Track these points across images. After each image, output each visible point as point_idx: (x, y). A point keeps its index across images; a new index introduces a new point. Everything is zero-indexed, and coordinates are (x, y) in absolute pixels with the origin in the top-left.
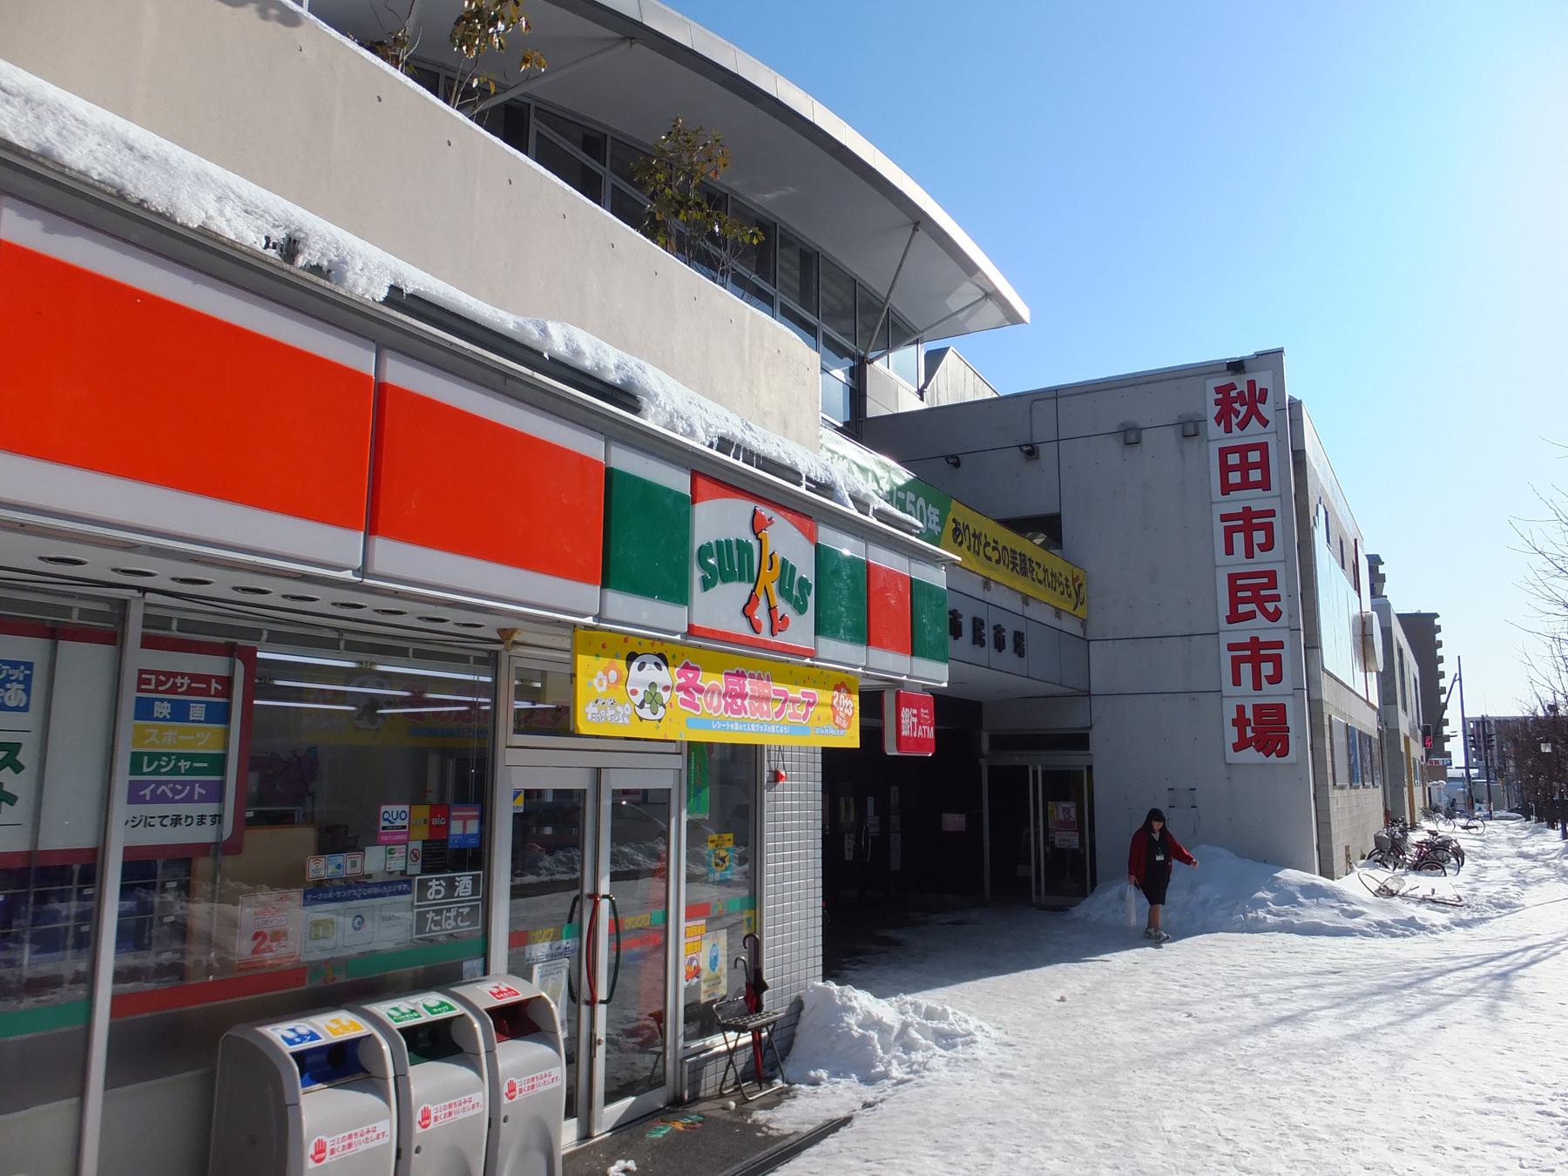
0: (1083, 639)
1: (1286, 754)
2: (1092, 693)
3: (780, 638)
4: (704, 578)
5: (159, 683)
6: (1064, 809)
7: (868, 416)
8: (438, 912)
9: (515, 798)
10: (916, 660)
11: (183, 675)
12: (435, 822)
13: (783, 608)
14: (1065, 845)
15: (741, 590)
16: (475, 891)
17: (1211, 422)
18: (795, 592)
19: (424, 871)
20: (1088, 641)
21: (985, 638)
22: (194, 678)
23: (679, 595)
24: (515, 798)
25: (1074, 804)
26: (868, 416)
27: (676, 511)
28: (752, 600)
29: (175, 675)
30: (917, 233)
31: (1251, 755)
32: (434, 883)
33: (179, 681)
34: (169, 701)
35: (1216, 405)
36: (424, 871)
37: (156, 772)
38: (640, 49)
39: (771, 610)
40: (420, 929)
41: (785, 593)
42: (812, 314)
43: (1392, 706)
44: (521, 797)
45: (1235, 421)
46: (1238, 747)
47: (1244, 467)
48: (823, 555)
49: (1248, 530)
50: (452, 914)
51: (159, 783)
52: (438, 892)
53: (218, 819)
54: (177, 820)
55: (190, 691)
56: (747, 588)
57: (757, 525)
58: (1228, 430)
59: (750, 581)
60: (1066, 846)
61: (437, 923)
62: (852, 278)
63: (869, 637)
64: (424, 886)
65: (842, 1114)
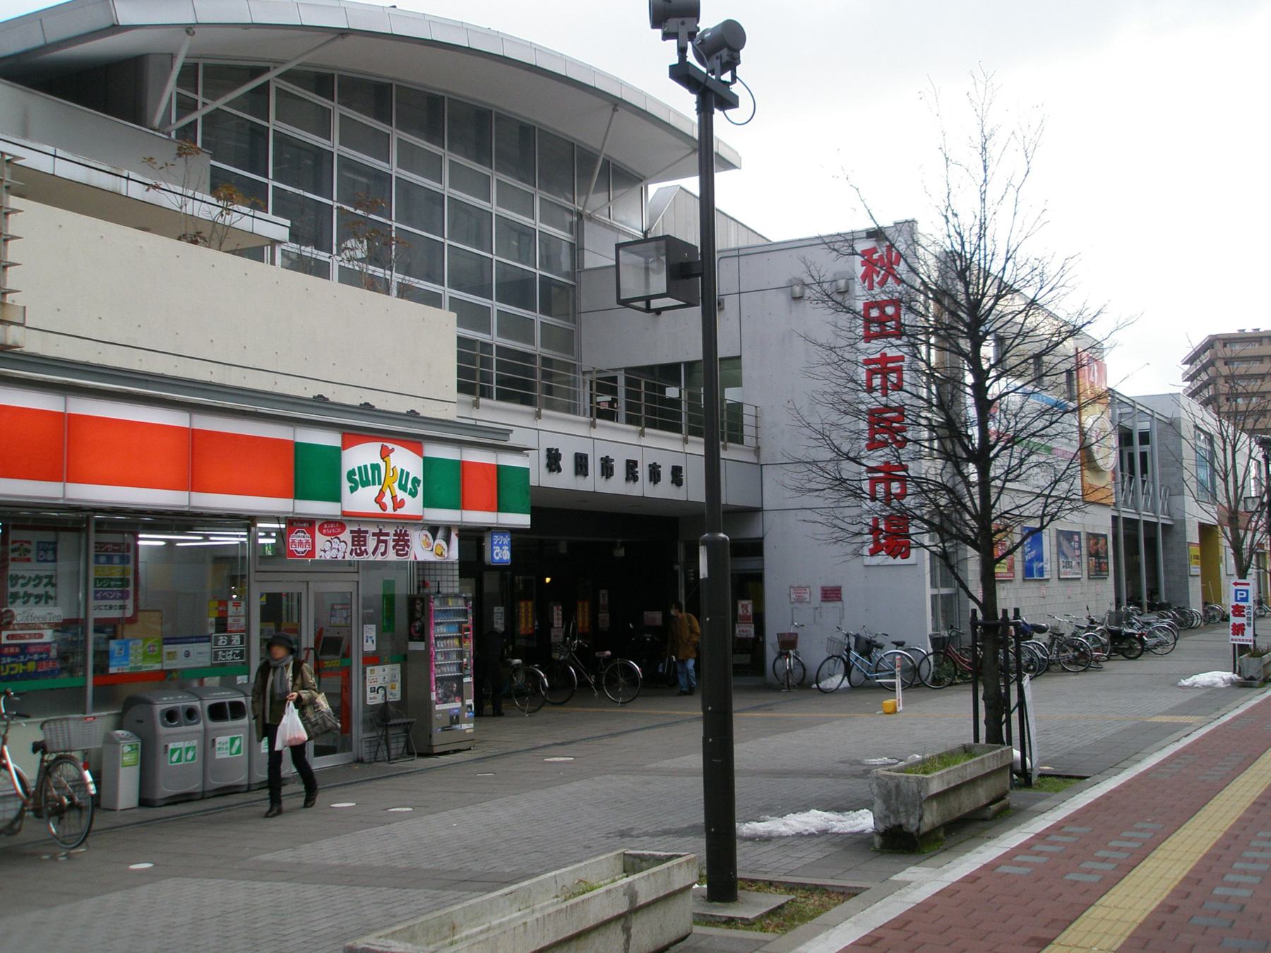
0: (757, 464)
1: (908, 557)
2: (764, 508)
3: (399, 512)
4: (351, 487)
5: (101, 548)
6: (743, 606)
7: (586, 267)
8: (224, 652)
9: (261, 597)
10: (500, 514)
11: (110, 543)
12: (221, 608)
13: (401, 495)
14: (744, 635)
15: (374, 490)
16: (242, 643)
17: (858, 280)
18: (409, 486)
19: (216, 632)
20: (761, 465)
21: (639, 475)
22: (115, 544)
23: (336, 497)
24: (261, 597)
25: (751, 601)
26: (586, 267)
27: (333, 456)
28: (382, 493)
29: (108, 543)
30: (616, 114)
31: (882, 558)
32: (221, 638)
33: (109, 546)
34: (106, 555)
35: (863, 266)
36: (216, 632)
37: (101, 587)
38: (351, 37)
39: (394, 498)
40: (216, 659)
41: (403, 487)
42: (529, 184)
43: (1178, 497)
44: (264, 597)
45: (876, 279)
46: (874, 553)
47: (359, 541)
48: (429, 463)
49: (885, 372)
50: (231, 653)
51: (103, 591)
52: (223, 642)
53: (123, 607)
54: (111, 607)
55: (114, 551)
56: (378, 488)
57: (385, 454)
58: (871, 287)
59: (379, 484)
60: (744, 636)
61: (224, 657)
62: (569, 142)
63: (463, 504)
64: (217, 640)
65: (682, 933)
